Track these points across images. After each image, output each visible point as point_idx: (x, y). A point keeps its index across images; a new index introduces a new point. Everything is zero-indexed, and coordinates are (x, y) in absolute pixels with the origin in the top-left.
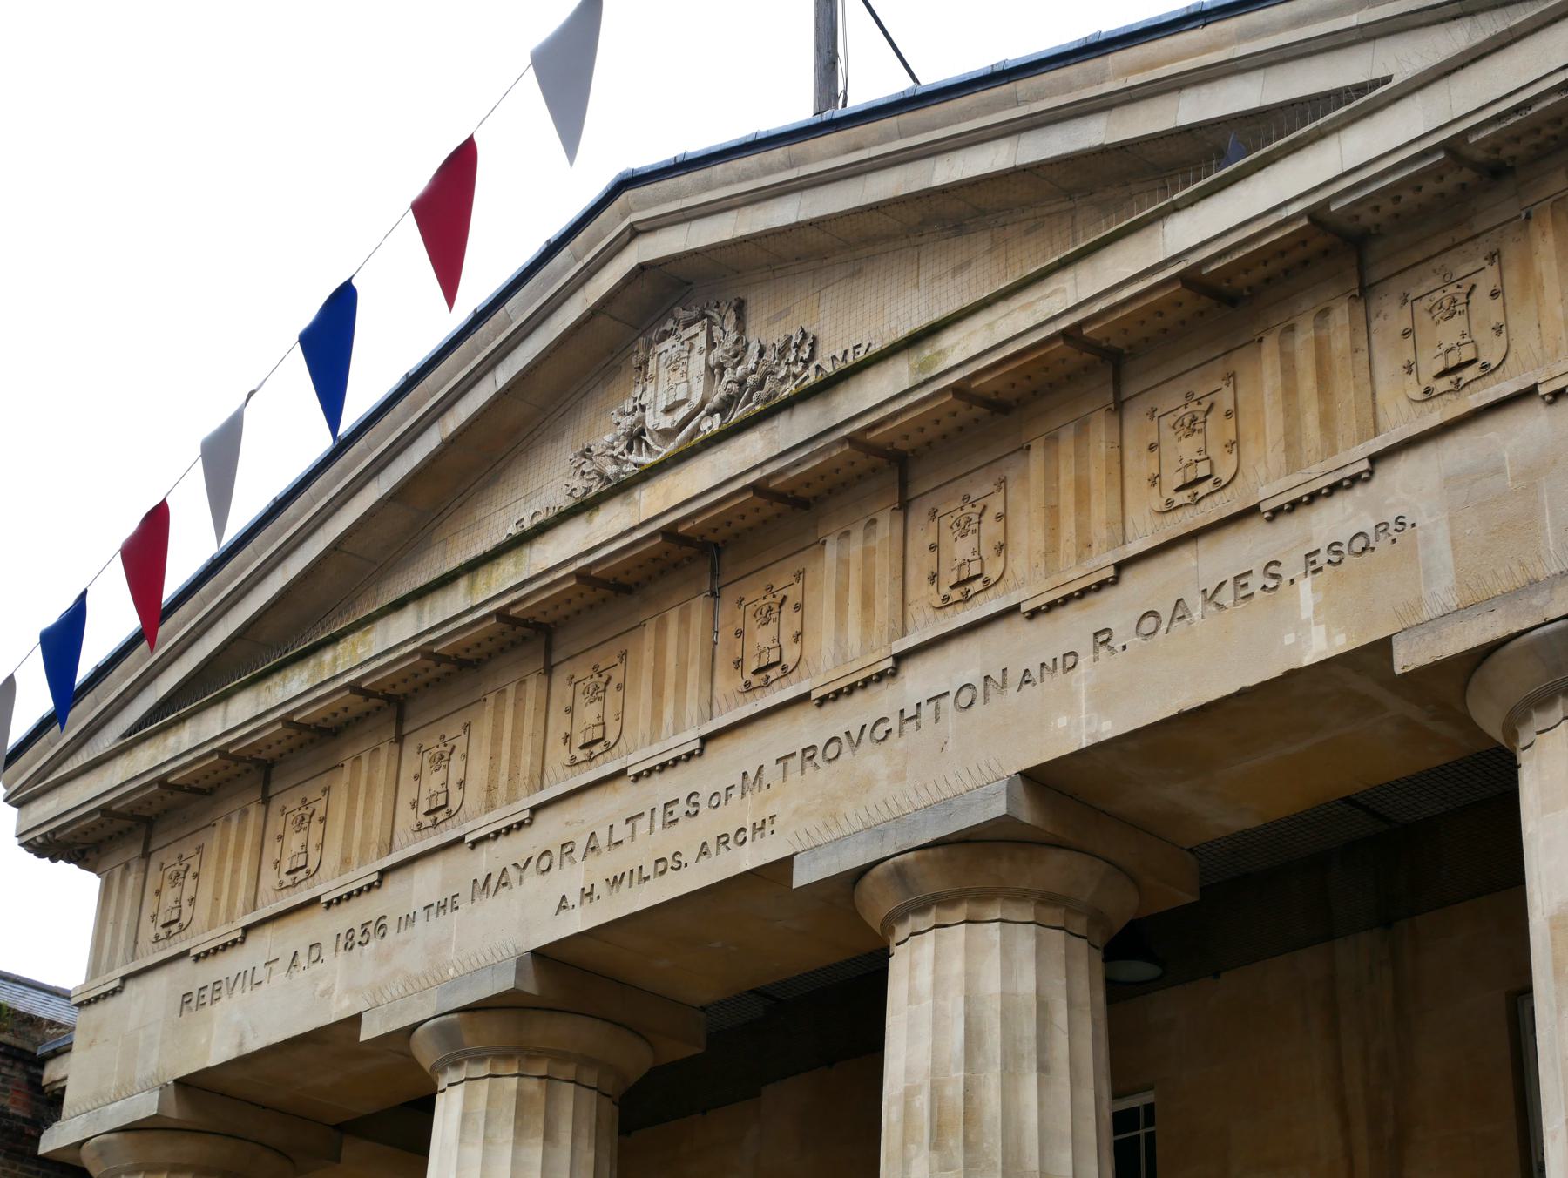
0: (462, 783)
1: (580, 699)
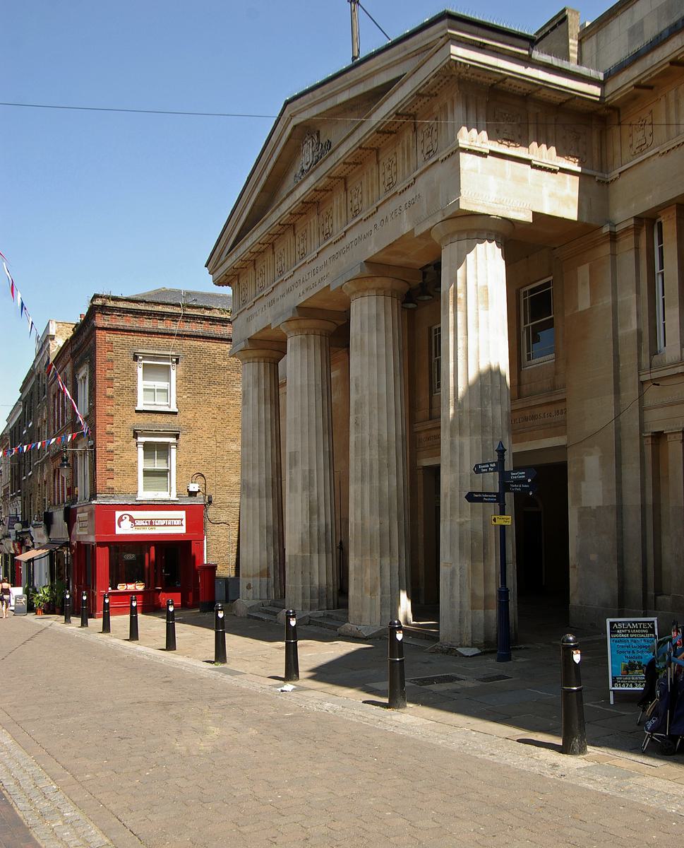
0: (332, 225)
1: (425, 138)
